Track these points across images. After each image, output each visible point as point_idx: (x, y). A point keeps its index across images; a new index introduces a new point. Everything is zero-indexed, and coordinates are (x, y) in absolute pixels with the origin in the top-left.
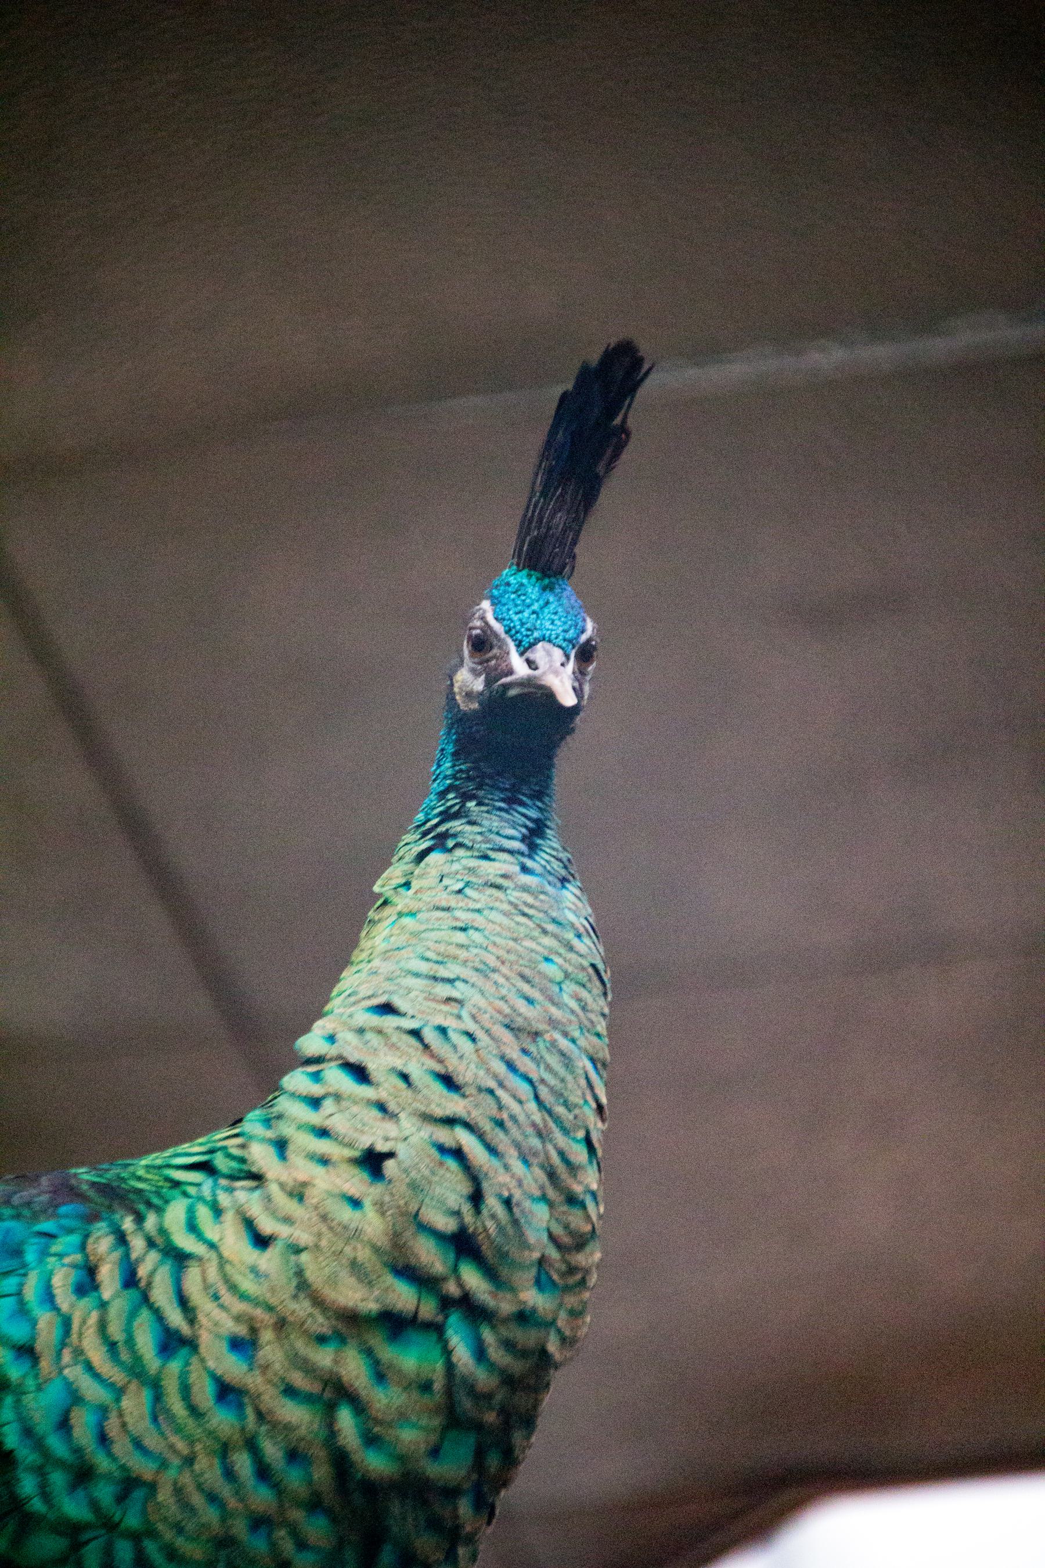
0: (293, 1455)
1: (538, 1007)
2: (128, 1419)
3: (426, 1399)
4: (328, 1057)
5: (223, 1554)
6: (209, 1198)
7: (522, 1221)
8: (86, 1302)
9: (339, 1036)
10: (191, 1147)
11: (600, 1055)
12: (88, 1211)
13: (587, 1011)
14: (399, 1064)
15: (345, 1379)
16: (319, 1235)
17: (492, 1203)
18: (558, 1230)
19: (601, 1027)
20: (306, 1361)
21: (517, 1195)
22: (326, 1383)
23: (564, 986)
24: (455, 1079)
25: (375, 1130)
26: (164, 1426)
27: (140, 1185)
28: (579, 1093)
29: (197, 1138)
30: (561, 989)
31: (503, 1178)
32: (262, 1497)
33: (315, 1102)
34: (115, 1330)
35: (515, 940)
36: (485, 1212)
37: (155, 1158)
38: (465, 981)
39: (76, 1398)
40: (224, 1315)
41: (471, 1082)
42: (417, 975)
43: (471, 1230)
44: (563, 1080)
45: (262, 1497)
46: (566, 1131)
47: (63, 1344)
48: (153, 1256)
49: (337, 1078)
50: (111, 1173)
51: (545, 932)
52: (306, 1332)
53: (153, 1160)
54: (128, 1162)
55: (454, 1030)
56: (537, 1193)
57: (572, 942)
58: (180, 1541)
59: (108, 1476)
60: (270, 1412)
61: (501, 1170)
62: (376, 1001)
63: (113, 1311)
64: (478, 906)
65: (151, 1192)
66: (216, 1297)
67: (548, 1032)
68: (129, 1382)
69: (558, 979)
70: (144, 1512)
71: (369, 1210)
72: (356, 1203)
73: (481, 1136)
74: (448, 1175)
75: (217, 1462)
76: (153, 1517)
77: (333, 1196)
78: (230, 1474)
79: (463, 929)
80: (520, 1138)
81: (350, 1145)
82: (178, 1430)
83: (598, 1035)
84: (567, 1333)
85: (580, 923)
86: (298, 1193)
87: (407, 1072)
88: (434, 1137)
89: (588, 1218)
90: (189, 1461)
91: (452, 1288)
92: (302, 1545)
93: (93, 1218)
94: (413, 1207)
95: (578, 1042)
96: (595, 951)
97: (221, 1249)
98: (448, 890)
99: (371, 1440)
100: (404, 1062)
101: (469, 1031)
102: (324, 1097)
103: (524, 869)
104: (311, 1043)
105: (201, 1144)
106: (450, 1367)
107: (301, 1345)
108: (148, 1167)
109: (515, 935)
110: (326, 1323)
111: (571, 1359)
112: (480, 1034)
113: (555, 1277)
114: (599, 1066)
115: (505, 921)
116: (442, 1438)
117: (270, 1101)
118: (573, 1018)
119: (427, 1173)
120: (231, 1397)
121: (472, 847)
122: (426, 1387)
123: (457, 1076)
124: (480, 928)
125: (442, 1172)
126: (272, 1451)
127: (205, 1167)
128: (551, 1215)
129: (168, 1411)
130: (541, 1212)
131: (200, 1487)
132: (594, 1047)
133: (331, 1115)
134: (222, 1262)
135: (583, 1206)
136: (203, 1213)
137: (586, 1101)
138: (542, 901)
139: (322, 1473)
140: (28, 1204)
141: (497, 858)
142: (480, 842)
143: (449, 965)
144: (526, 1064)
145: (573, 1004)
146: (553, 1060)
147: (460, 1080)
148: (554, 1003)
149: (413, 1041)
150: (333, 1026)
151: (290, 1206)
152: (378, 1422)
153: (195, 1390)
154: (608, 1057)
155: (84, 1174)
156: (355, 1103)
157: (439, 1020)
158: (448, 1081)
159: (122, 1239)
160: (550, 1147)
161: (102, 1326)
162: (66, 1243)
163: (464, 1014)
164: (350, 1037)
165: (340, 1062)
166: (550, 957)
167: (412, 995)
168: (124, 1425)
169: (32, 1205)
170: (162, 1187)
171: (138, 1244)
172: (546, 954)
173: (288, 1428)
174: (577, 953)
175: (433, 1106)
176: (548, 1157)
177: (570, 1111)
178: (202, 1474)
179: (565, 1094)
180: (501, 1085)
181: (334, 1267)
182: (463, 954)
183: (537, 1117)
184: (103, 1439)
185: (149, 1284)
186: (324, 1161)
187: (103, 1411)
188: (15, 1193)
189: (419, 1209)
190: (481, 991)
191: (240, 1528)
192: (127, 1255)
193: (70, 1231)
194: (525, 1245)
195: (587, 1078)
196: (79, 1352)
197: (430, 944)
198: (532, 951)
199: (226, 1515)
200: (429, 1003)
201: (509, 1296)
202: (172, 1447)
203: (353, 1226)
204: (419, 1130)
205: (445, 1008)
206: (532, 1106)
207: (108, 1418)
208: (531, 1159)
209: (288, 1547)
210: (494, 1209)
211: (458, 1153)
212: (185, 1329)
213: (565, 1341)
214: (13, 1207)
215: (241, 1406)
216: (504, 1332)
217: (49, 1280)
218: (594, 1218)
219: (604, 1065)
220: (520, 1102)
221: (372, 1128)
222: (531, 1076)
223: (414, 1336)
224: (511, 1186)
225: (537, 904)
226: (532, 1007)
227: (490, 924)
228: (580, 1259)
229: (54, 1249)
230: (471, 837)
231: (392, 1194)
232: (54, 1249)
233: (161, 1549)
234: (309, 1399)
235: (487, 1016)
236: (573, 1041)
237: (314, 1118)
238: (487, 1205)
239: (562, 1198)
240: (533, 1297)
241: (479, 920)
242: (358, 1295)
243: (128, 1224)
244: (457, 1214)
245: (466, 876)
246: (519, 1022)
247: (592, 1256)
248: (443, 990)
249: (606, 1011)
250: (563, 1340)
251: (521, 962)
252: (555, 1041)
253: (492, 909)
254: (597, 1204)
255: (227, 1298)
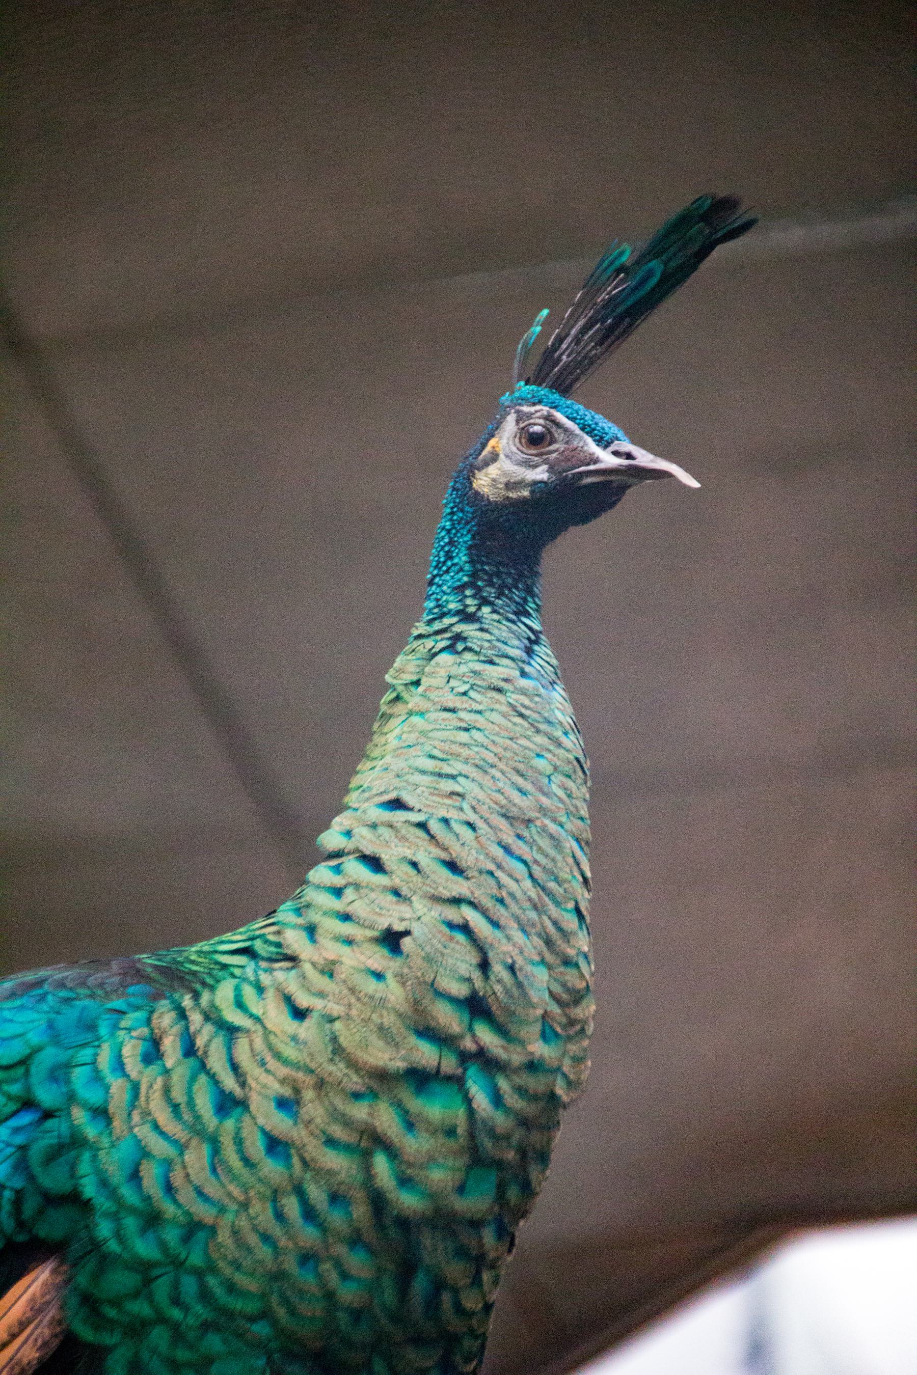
0: (335, 1198)
1: (530, 797)
2: (190, 1171)
3: (451, 1143)
4: (346, 851)
5: (275, 1286)
6: (252, 979)
7: (525, 983)
8: (153, 1070)
9: (355, 831)
10: (233, 935)
11: (584, 836)
12: (153, 990)
13: (573, 798)
14: (408, 853)
15: (379, 1130)
16: (350, 1006)
17: (498, 969)
18: (557, 989)
19: (584, 812)
20: (344, 1115)
21: (520, 962)
22: (362, 1133)
23: (553, 778)
24: (458, 864)
25: (391, 912)
26: (222, 1177)
27: (194, 968)
28: (568, 870)
29: (237, 928)
30: (550, 780)
31: (507, 947)
32: (309, 1235)
33: (338, 892)
34: (178, 1095)
35: (511, 739)
36: (492, 977)
37: (205, 946)
38: (467, 777)
39: (145, 1153)
40: (271, 1078)
41: (473, 866)
42: (423, 772)
43: (481, 994)
44: (553, 860)
45: (309, 1235)
46: (558, 904)
47: (133, 1106)
48: (209, 1028)
49: (355, 869)
50: (171, 955)
51: (538, 731)
52: (343, 1090)
53: (202, 947)
54: (183, 948)
55: (456, 821)
56: (537, 958)
57: (560, 739)
58: (238, 1277)
59: (175, 1222)
60: (313, 1159)
61: (504, 941)
62: (386, 798)
63: (175, 1077)
64: (479, 707)
65: (204, 973)
66: (263, 1063)
67: (538, 818)
68: (191, 1138)
69: (548, 773)
70: (206, 1254)
71: (391, 981)
72: (379, 976)
73: (484, 913)
74: (458, 947)
75: (269, 1206)
76: (214, 1256)
77: (362, 971)
78: (280, 1216)
79: (466, 730)
80: (519, 912)
81: (371, 927)
82: (235, 1178)
83: (582, 819)
84: (572, 1077)
85: (567, 720)
86: (329, 970)
87: (417, 861)
88: (443, 915)
89: (582, 976)
90: (245, 1205)
91: (468, 1044)
92: (345, 1276)
93: (157, 996)
94: (429, 978)
95: (565, 826)
96: (578, 746)
97: (266, 1021)
98: (454, 692)
99: (404, 1181)
100: (413, 852)
101: (470, 820)
102: (345, 887)
103: (523, 674)
104: (331, 839)
105: (240, 933)
106: (471, 1112)
107: (339, 1102)
108: (199, 953)
109: (512, 734)
110: (360, 1081)
111: (579, 1098)
112: (480, 824)
113: (558, 1029)
114: (583, 844)
115: (503, 722)
116: (467, 1176)
117: (299, 894)
118: (561, 805)
119: (439, 946)
120: (280, 1148)
121: (480, 652)
122: (451, 1132)
123: (460, 861)
124: (481, 728)
125: (452, 945)
126: (317, 1194)
127: (246, 951)
128: (550, 976)
129: (225, 1163)
130: (542, 974)
131: (255, 1228)
132: (579, 829)
133: (353, 901)
134: (267, 1032)
135: (577, 965)
136: (249, 992)
137: (574, 877)
138: (536, 703)
139: (361, 1212)
140: (101, 985)
141: (501, 663)
142: (486, 649)
143: (451, 762)
144: (520, 848)
145: (560, 793)
146: (545, 843)
147: (463, 864)
148: (545, 794)
149: (421, 833)
150: (349, 822)
151: (322, 982)
152: (410, 1165)
153: (248, 1143)
154: (590, 836)
155: (147, 960)
156: (372, 890)
157: (443, 813)
158: (453, 866)
159: (182, 1014)
160: (545, 918)
161: (167, 1091)
162: (133, 1018)
163: (465, 806)
164: (365, 831)
165: (357, 855)
166: (542, 754)
167: (419, 791)
168: (187, 1175)
169: (105, 986)
170: (213, 969)
171: (196, 1018)
172: (538, 751)
173: (330, 1173)
174: (565, 749)
175: (441, 889)
176: (544, 927)
177: (560, 885)
178: (256, 1218)
179: (556, 872)
180: (499, 866)
181: (365, 1032)
182: (465, 752)
183: (533, 893)
184: (169, 1188)
185: (206, 1053)
186: (349, 941)
187: (168, 1164)
188: (89, 976)
189: (435, 978)
190: (479, 784)
191: (290, 1264)
192: (187, 1028)
193: (137, 1008)
194: (531, 1005)
195: (574, 857)
196: (146, 1113)
197: (436, 743)
198: (526, 748)
199: (277, 1251)
200: (434, 798)
201: (519, 1049)
202: (229, 1194)
203: (378, 996)
204: (430, 910)
205: (448, 801)
206: (528, 883)
207: (173, 1170)
208: (528, 929)
209: (333, 1278)
210: (500, 975)
211: (465, 928)
212: (238, 1092)
213: (570, 1084)
214: (89, 988)
215: (288, 1157)
216: (518, 1081)
217: (120, 1050)
218: (588, 977)
219: (587, 843)
220: (517, 881)
221: (389, 911)
222: (524, 857)
223: (436, 1087)
224: (513, 954)
225: (532, 705)
226: (524, 797)
227: (490, 724)
228: (578, 1012)
229: (123, 1025)
230: (479, 643)
231: (410, 968)
232: (123, 1024)
233: (221, 1283)
234: (348, 1148)
235: (485, 807)
236: (561, 825)
237: (337, 905)
238: (494, 972)
239: (558, 961)
240: (540, 1049)
241: (480, 720)
242: (386, 1056)
243: (187, 1001)
244: (469, 980)
245: (472, 679)
246: (514, 811)
247: (588, 1008)
248: (447, 786)
249: (588, 796)
250: (569, 1083)
251: (516, 758)
252: (546, 826)
253: (492, 710)
254: (589, 963)
255: (272, 1064)
